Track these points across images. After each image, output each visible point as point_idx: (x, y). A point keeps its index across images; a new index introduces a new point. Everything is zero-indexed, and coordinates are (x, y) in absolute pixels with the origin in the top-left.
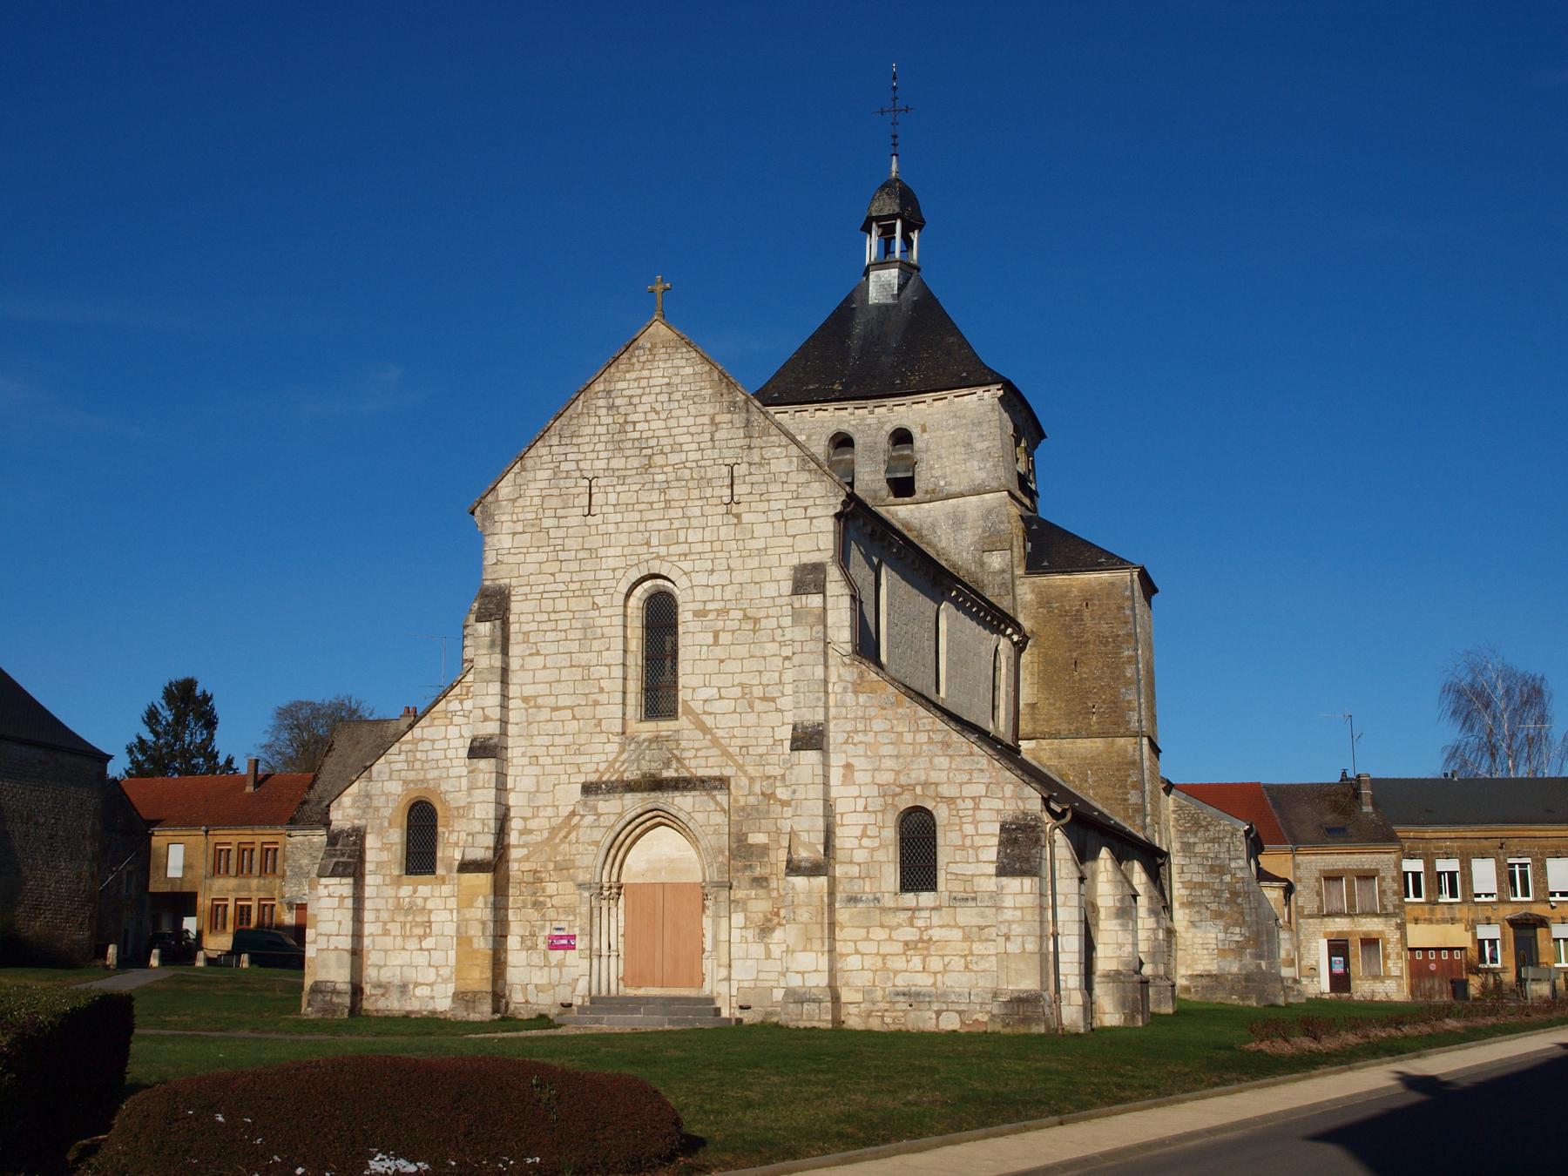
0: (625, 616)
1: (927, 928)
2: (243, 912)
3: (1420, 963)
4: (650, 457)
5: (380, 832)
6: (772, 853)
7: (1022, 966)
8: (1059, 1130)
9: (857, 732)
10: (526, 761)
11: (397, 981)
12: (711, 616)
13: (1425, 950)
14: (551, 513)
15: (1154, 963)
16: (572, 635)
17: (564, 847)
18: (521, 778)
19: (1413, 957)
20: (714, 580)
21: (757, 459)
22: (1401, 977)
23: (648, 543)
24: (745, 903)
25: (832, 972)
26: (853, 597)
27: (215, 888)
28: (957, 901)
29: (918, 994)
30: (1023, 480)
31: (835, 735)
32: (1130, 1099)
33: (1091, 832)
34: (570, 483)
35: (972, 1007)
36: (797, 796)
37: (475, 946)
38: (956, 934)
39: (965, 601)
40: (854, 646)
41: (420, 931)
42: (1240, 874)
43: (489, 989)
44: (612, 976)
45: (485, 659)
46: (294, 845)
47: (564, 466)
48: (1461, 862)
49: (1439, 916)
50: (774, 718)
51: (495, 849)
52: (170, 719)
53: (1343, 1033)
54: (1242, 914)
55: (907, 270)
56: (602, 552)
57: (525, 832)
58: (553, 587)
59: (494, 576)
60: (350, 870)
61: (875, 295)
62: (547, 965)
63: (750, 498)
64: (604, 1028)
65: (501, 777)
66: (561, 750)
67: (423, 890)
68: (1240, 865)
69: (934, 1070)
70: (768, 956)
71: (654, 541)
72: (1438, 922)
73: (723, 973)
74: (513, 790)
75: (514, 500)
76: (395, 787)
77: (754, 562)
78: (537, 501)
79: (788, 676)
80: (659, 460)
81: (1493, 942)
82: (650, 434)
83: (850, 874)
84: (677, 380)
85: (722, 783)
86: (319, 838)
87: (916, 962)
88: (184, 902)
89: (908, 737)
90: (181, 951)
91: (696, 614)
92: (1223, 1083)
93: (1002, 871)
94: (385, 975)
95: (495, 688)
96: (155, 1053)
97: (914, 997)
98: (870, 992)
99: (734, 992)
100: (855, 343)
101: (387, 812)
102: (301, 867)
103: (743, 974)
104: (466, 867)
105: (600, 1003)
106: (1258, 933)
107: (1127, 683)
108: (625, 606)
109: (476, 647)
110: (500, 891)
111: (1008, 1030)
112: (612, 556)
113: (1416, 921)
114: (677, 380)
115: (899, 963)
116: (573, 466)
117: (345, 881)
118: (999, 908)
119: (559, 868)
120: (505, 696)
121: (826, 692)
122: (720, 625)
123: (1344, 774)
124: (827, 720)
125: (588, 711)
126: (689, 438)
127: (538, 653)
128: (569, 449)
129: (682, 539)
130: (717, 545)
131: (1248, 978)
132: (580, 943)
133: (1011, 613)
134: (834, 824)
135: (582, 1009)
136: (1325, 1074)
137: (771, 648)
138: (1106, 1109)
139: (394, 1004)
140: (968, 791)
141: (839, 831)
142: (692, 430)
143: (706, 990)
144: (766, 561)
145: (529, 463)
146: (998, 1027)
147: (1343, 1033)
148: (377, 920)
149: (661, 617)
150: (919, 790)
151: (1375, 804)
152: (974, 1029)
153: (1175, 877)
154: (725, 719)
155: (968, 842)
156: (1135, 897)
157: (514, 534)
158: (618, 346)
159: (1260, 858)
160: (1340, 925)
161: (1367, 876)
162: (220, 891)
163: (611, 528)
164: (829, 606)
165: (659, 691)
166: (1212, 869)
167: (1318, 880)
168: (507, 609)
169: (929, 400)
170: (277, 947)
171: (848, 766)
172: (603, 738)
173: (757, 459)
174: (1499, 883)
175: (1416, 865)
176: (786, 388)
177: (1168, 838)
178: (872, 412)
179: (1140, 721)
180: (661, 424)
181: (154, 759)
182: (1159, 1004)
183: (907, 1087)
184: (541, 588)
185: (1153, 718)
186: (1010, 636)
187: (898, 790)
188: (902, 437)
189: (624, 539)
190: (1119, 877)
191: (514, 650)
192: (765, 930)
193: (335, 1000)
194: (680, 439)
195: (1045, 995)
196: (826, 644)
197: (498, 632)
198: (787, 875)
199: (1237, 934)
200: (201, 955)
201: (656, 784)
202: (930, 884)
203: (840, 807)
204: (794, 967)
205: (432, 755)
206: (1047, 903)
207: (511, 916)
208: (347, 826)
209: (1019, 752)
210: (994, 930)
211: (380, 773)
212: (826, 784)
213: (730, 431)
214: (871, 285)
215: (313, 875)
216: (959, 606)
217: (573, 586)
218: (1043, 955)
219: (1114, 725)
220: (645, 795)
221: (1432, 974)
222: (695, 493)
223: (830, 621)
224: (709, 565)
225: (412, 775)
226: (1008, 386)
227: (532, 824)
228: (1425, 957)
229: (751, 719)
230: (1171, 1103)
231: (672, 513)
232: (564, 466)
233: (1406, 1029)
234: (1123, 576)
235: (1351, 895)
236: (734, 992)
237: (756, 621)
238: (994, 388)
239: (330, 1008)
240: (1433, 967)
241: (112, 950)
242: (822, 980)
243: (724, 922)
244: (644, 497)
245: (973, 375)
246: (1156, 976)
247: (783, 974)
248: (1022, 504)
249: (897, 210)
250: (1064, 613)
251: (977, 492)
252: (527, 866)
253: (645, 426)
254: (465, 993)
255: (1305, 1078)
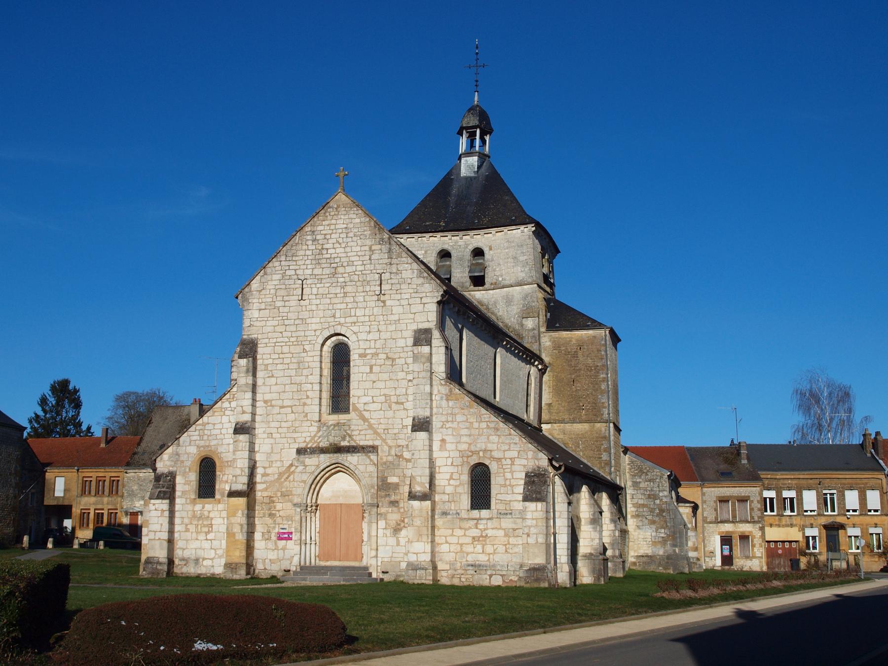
0: (321, 356)
1: (485, 529)
2: (99, 517)
3: (773, 549)
4: (336, 268)
5: (184, 474)
6: (401, 488)
7: (536, 550)
8: (543, 636)
9: (448, 422)
10: (265, 436)
11: (193, 557)
12: (368, 357)
13: (776, 542)
14: (281, 298)
15: (613, 549)
16: (291, 366)
17: (287, 483)
18: (263, 445)
19: (769, 546)
20: (370, 337)
21: (394, 271)
22: (761, 557)
23: (334, 316)
24: (386, 515)
25: (433, 553)
26: (447, 348)
27: (82, 503)
28: (502, 514)
29: (480, 566)
30: (546, 278)
31: (436, 423)
32: (584, 621)
33: (577, 476)
34: (291, 282)
35: (509, 572)
36: (415, 457)
37: (237, 538)
38: (501, 533)
39: (511, 347)
40: (447, 375)
41: (206, 529)
42: (665, 500)
43: (244, 561)
44: (312, 555)
45: (244, 380)
46: (129, 478)
47: (288, 273)
48: (777, 493)
49: (784, 523)
50: (402, 414)
51: (248, 485)
52: (54, 403)
53: (711, 587)
54: (666, 522)
55: (483, 157)
56: (309, 321)
57: (265, 475)
58: (282, 340)
59: (249, 333)
60: (167, 496)
61: (464, 172)
62: (277, 548)
63: (391, 292)
64: (308, 583)
65: (252, 444)
66: (285, 430)
67: (208, 506)
68: (665, 493)
69: (483, 606)
70: (398, 544)
71: (338, 315)
72: (784, 526)
73: (373, 553)
74: (258, 452)
75: (260, 291)
76: (193, 450)
77: (392, 328)
78: (273, 291)
79: (411, 391)
80: (341, 270)
81: (814, 538)
82: (336, 255)
83: (444, 499)
84: (351, 226)
85: (374, 449)
86: (146, 474)
87: (479, 548)
88: (65, 511)
89: (476, 425)
90: (65, 540)
91: (360, 355)
92: (637, 613)
93: (526, 499)
94: (187, 554)
95: (249, 395)
96: (79, 595)
97: (477, 567)
98: (453, 564)
99: (379, 564)
100: (452, 199)
101: (188, 464)
102: (133, 491)
103: (385, 554)
104: (232, 494)
105: (305, 569)
106: (674, 533)
107: (602, 392)
108: (321, 351)
109: (239, 373)
110: (251, 508)
111: (528, 585)
112: (314, 323)
113: (771, 525)
114: (351, 226)
115: (470, 549)
116: (293, 272)
117: (164, 501)
118: (524, 519)
119: (283, 495)
120: (254, 400)
121: (431, 400)
122: (373, 362)
123: (732, 441)
124: (431, 415)
125: (300, 409)
126: (357, 258)
127: (273, 376)
128: (290, 263)
129: (353, 314)
130: (372, 318)
131: (669, 557)
132: (295, 537)
133: (537, 353)
134: (435, 472)
135: (295, 573)
136: (695, 610)
137: (401, 375)
138: (570, 626)
139: (191, 570)
140: (509, 454)
141: (437, 476)
142: (359, 254)
143: (364, 563)
144: (399, 327)
145: (268, 270)
146: (522, 584)
147: (711, 587)
148: (182, 523)
149: (341, 357)
150: (481, 454)
151: (748, 459)
152: (509, 585)
153: (629, 501)
154: (375, 414)
155: (508, 483)
156: (601, 513)
157: (260, 310)
158: (318, 206)
159: (680, 490)
160: (728, 528)
161: (743, 500)
162: (85, 504)
163: (314, 307)
164: (433, 352)
165: (339, 399)
166: (649, 497)
167: (715, 502)
168: (256, 351)
169: (493, 232)
170: (124, 537)
171: (443, 440)
172: (309, 423)
173: (394, 271)
174: (818, 504)
175: (772, 494)
176: (416, 224)
177: (625, 479)
178: (461, 239)
179: (609, 414)
180: (342, 250)
181: (45, 427)
182: (615, 571)
183: (466, 614)
184: (275, 340)
185: (617, 412)
186: (537, 366)
187: (470, 454)
188: (478, 253)
189: (321, 314)
190: (592, 502)
191: (260, 374)
192: (397, 530)
193: (159, 567)
194: (352, 259)
195: (549, 566)
196: (432, 373)
197: (251, 365)
198: (409, 500)
199: (663, 533)
200: (76, 541)
201: (338, 449)
202: (487, 506)
203: (438, 463)
204: (412, 550)
205: (214, 432)
206: (550, 516)
207: (257, 521)
208: (166, 471)
209: (541, 431)
210: (521, 531)
211: (184, 442)
212: (431, 450)
213: (380, 255)
214: (462, 165)
215: (147, 498)
216: (508, 350)
217: (292, 339)
218: (548, 545)
219: (594, 416)
220: (331, 455)
221: (779, 556)
222: (360, 289)
223: (434, 360)
224: (367, 329)
225: (202, 443)
226: (538, 225)
227: (269, 471)
228: (776, 546)
229: (390, 414)
230: (606, 623)
231: (348, 300)
232: (288, 273)
233: (749, 586)
234: (602, 333)
235: (734, 510)
236: (379, 564)
237: (393, 360)
238: (530, 226)
239: (157, 572)
240: (780, 552)
241: (26, 539)
242: (427, 558)
243: (374, 525)
244: (333, 290)
245: (518, 218)
246: (613, 557)
247: (406, 554)
248: (545, 291)
249: (477, 123)
250: (567, 353)
251: (520, 284)
252: (265, 494)
253: (332, 251)
254: (231, 564)
255: (684, 611)
